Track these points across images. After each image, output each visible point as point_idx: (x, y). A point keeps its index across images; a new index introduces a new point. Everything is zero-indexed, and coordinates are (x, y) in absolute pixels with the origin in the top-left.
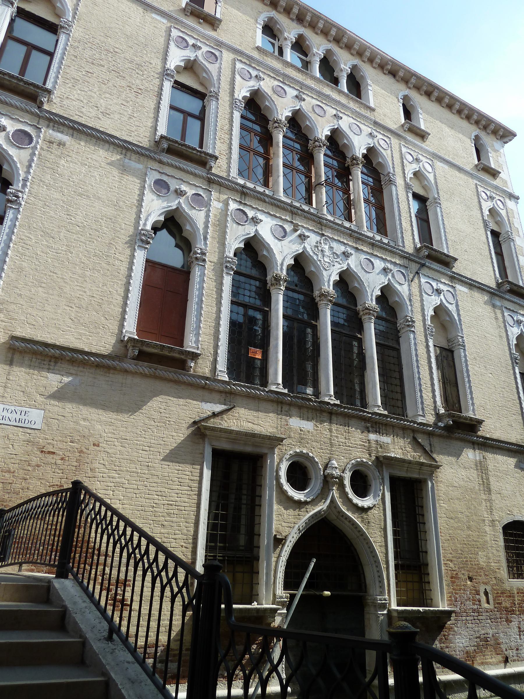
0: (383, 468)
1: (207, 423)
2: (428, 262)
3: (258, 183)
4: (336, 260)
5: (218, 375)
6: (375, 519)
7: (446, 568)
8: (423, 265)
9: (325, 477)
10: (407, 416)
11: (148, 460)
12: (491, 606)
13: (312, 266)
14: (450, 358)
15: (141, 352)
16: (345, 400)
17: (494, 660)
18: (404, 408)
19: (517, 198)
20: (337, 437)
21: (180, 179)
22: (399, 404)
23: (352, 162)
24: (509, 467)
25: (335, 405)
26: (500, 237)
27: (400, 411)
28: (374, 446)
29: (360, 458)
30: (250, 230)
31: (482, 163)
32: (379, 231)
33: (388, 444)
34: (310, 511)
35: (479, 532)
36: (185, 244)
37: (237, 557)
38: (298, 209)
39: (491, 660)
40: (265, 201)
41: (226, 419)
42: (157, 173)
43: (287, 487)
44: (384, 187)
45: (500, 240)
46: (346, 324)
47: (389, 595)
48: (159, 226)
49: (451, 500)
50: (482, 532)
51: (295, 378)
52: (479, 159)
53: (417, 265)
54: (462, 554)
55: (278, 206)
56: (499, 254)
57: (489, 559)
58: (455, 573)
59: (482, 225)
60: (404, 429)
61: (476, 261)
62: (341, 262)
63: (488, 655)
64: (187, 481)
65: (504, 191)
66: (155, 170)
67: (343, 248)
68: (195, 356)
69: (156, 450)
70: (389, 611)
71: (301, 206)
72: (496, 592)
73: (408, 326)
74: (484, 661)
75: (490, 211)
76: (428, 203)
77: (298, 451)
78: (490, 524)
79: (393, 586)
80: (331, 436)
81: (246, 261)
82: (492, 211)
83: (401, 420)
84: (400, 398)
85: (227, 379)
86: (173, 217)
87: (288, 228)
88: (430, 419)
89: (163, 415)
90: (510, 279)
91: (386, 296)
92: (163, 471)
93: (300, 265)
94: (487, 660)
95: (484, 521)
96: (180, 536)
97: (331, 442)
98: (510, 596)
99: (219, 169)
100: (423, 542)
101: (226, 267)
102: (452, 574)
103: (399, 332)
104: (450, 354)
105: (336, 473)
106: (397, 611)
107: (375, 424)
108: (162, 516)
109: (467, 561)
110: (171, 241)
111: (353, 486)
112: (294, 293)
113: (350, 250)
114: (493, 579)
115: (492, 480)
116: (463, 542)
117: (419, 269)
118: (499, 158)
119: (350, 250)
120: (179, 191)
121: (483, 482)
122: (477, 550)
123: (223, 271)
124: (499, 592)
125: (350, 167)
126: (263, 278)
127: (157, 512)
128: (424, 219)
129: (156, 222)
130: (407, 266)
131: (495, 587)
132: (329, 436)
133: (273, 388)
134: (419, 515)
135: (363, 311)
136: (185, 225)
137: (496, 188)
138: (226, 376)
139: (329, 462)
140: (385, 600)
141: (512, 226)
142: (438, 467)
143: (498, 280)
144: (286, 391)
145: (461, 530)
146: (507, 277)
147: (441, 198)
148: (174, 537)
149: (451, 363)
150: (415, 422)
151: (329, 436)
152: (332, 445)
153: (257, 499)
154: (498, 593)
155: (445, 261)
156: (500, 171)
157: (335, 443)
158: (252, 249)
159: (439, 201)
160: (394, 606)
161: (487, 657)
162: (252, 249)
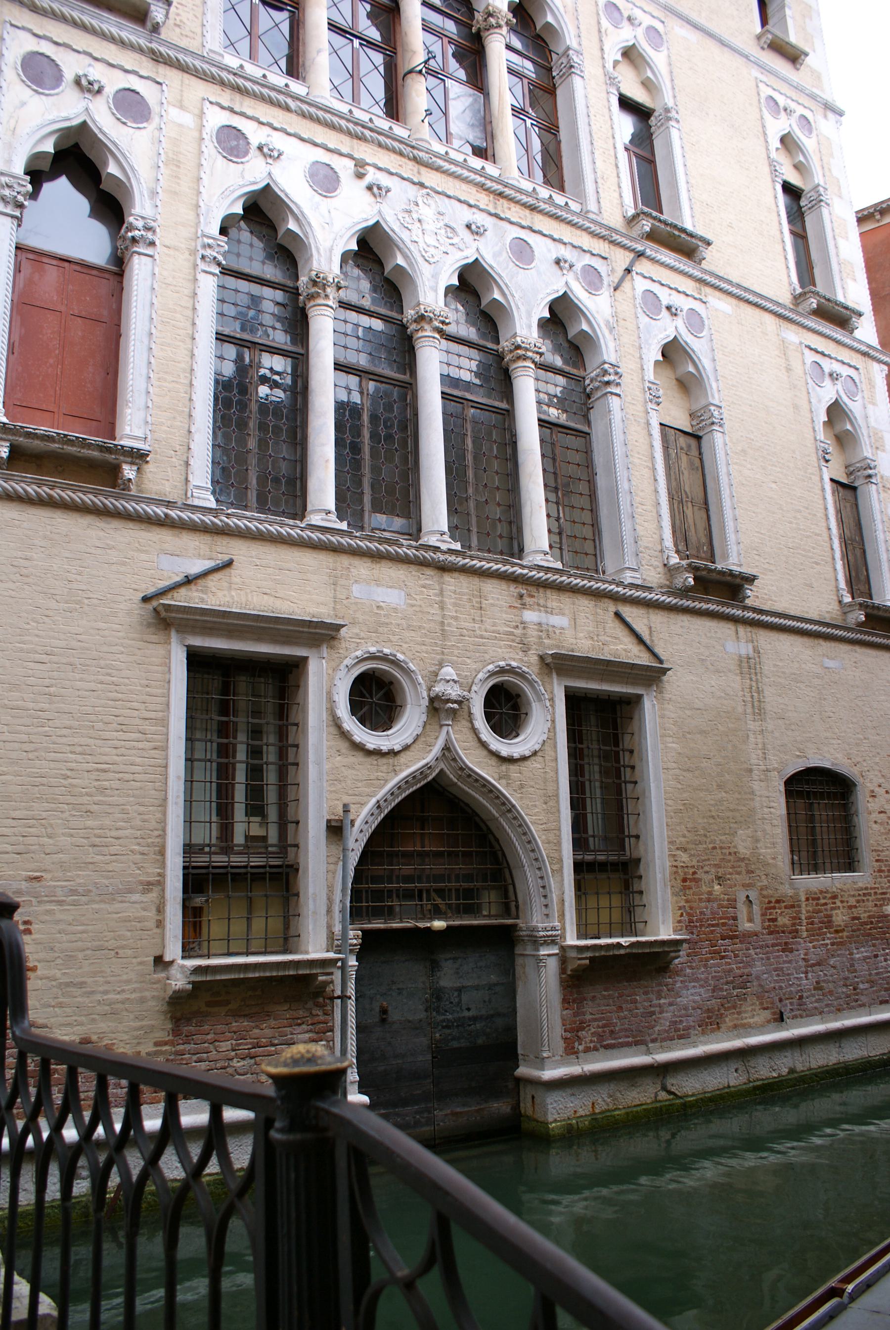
0: (552, 683)
1: (173, 598)
2: (651, 249)
3: (275, 68)
4: (451, 241)
5: (192, 496)
6: (532, 778)
7: (675, 864)
8: (640, 255)
9: (432, 700)
10: (604, 573)
11: (47, 682)
13: (395, 248)
14: (694, 452)
15: (14, 450)
16: (474, 542)
17: (756, 1019)
18: (597, 554)
19: (841, 114)
20: (456, 618)
21: (86, 53)
22: (588, 547)
23: (485, 20)
24: (803, 666)
25: (451, 551)
26: (803, 199)
27: (589, 562)
28: (535, 633)
29: (505, 660)
30: (253, 174)
31: (768, 31)
32: (547, 182)
33: (563, 629)
34: (401, 771)
35: (740, 793)
36: (110, 207)
37: (252, 867)
38: (363, 127)
39: (751, 1021)
40: (288, 109)
41: (214, 589)
42: (29, 36)
43: (351, 724)
44: (557, 81)
45: (802, 204)
46: (477, 381)
47: (562, 915)
48: (46, 166)
49: (689, 736)
50: (745, 793)
51: (367, 499)
52: (764, 21)
53: (627, 253)
54: (705, 836)
55: (318, 121)
56: (800, 236)
57: (757, 841)
58: (691, 871)
59: (766, 169)
60: (597, 595)
61: (750, 245)
62: (462, 246)
63: (745, 1012)
64: (137, 721)
65: (813, 97)
66: (23, 28)
67: (467, 215)
68: (138, 457)
69: (64, 661)
70: (563, 948)
71: (371, 120)
72: (767, 900)
73: (608, 383)
74: (739, 1022)
75: (783, 140)
76: (653, 121)
78: (762, 777)
79: (570, 885)
80: (444, 616)
81: (251, 245)
82: (787, 141)
84: (589, 535)
85: (213, 504)
86: (76, 146)
87: (344, 167)
88: (653, 576)
89: (75, 586)
91: (560, 317)
92: (81, 703)
93: (370, 249)
94: (745, 1021)
95: (751, 771)
96: (127, 832)
97: (443, 630)
98: (793, 906)
99: (178, 30)
100: (632, 819)
101: (203, 257)
102: (685, 873)
103: (589, 396)
104: (693, 442)
105: (454, 692)
106: (580, 949)
108: (87, 794)
109: (714, 848)
110: (81, 204)
111: (489, 717)
112: (361, 316)
113: (480, 219)
114: (763, 877)
115: (769, 693)
116: (709, 814)
117: (632, 263)
118: (807, 20)
119: (480, 219)
120: (84, 82)
121: (752, 697)
122: (735, 826)
123: (195, 266)
124: (773, 900)
125: (482, 34)
126: (290, 283)
127: (75, 786)
128: (645, 150)
129: (36, 157)
130: (606, 255)
131: (765, 893)
132: (439, 619)
133: (315, 519)
135: (511, 351)
136: (106, 164)
137: (798, 88)
138: (212, 498)
139: (439, 670)
140: (553, 929)
141: (827, 173)
142: (665, 671)
143: (794, 290)
144: (344, 526)
145: (707, 790)
147: (681, 108)
148: (114, 833)
149: (697, 462)
150: (619, 584)
151: (439, 619)
152: (444, 634)
153: (292, 751)
154: (770, 902)
155: (684, 245)
156: (807, 49)
157: (452, 632)
158: (261, 213)
159: (676, 116)
160: (572, 940)
161: (744, 1015)
162: (261, 213)
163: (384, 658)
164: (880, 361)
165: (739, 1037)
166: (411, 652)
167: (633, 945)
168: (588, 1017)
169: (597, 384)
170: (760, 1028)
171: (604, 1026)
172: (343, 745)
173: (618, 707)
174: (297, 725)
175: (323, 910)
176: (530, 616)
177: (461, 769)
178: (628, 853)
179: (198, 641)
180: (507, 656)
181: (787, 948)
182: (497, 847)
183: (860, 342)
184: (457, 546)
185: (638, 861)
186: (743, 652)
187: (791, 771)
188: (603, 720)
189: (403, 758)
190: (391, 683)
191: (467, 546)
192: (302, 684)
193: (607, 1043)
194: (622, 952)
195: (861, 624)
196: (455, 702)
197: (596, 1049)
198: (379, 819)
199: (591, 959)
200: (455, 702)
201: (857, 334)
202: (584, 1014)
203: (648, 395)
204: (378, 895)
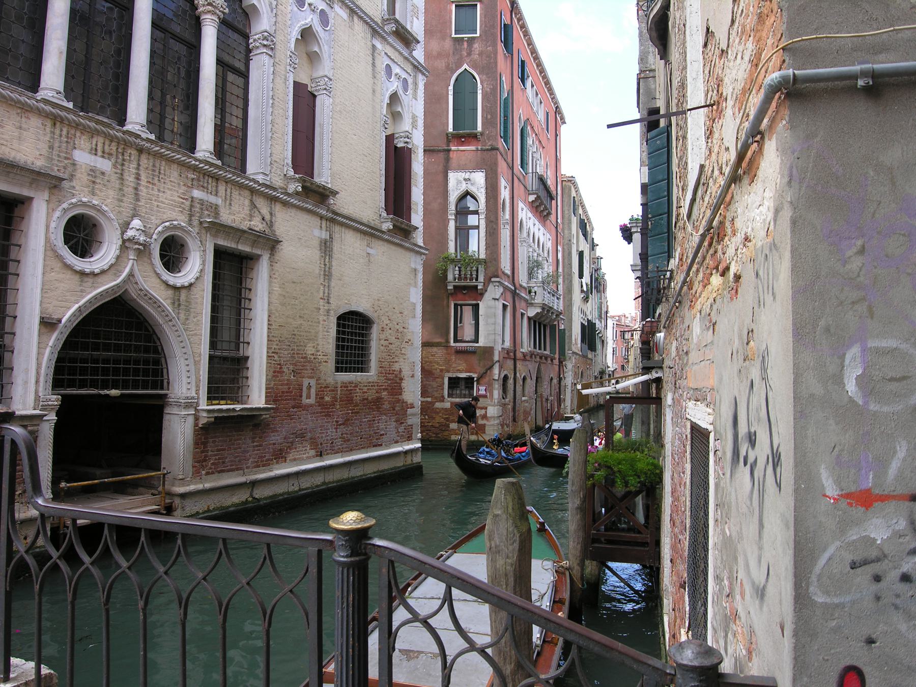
12: (312, 401)
25: (148, 140)
28: (198, 206)
60: (242, 187)
77: (84, 200)
83: (239, 176)
90: (397, 16)
103: (250, 51)
106: (209, 411)
107: (204, 175)
111: (162, 256)
134: (245, 299)
135: (204, 5)
140: (193, 398)
146: (394, 14)
163: (94, 207)
164: (423, 74)
165: (297, 465)
166: (105, 203)
167: (242, 410)
168: (210, 453)
169: (258, 44)
170: (309, 459)
171: (219, 459)
172: (58, 265)
173: (245, 261)
174: (20, 246)
175: (33, 380)
176: (197, 194)
177: (141, 290)
178: (241, 351)
179: (221, 242)
180: (179, 218)
181: (328, 415)
182: (158, 344)
183: (414, 58)
184: (153, 137)
185: (247, 358)
186: (323, 237)
187: (341, 311)
188: (232, 269)
189: (100, 279)
190: (95, 225)
191: (160, 138)
192: (26, 217)
193: (220, 469)
194: (236, 414)
195: (389, 231)
196: (141, 244)
197: (213, 473)
198: (79, 319)
199: (216, 418)
200: (141, 244)
201: (415, 53)
202: (207, 452)
203: (288, 60)
204: (72, 371)
